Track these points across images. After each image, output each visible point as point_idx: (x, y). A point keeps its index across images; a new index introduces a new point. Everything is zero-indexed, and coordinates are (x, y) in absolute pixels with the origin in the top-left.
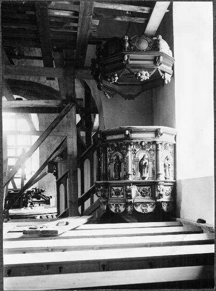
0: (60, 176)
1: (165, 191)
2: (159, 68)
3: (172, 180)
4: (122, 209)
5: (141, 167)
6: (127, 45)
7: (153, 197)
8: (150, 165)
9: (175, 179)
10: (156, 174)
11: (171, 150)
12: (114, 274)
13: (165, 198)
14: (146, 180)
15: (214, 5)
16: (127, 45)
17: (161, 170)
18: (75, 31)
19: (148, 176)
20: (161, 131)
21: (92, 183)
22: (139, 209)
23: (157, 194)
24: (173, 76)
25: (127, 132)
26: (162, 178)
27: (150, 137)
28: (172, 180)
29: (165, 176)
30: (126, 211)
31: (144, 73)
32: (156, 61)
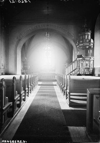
4: (83, 73)
5: (87, 65)
9: (93, 67)
10: (90, 66)
11: (93, 61)
19: (88, 67)
20: (91, 58)
23: (90, 70)
27: (89, 59)
29: (92, 67)
30: (83, 74)
31: (87, 46)
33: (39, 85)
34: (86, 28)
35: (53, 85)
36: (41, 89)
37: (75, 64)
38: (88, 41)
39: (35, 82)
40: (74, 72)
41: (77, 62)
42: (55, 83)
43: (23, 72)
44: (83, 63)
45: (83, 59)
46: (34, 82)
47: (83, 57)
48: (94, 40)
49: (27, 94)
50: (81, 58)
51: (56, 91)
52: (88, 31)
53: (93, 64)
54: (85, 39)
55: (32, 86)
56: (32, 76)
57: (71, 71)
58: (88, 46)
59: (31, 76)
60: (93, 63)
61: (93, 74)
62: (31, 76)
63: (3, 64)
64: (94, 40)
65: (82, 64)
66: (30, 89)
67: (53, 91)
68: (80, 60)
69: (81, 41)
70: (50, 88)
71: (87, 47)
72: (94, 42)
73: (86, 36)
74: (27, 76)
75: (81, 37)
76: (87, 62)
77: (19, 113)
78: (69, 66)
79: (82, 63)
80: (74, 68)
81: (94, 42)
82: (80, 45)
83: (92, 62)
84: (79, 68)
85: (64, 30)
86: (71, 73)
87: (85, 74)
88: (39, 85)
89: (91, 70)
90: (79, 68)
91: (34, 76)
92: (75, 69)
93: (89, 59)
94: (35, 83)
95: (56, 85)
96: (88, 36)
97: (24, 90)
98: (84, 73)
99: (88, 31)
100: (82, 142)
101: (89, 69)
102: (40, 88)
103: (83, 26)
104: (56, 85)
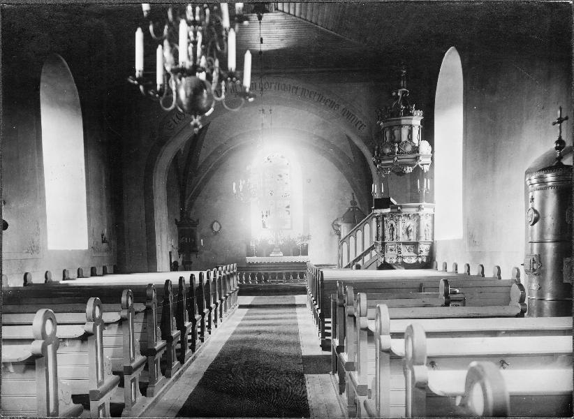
0: (342, 237)
1: (424, 248)
2: (419, 163)
3: (431, 240)
4: (394, 261)
5: (408, 232)
6: (397, 150)
7: (415, 252)
8: (414, 230)
9: (433, 239)
10: (418, 235)
11: (430, 218)
12: (483, 341)
13: (425, 253)
14: (412, 241)
15: (42, 284)
16: (397, 150)
17: (422, 233)
18: (182, 228)
19: (413, 238)
20: (423, 207)
21: (371, 241)
22: (406, 261)
23: (419, 251)
24: (432, 165)
25: (399, 208)
26: (423, 239)
27: (413, 211)
28: (431, 240)
29: (425, 238)
30: (397, 262)
31: (408, 168)
32: (417, 159)
33: (241, 307)
34: (405, 101)
35: (294, 306)
36: (248, 319)
37: (363, 234)
38: (409, 148)
39: (227, 295)
40: (367, 258)
41: (377, 222)
42: (299, 299)
43: (173, 261)
44: (394, 224)
45: (396, 210)
46: (225, 293)
47: (392, 204)
48: (432, 144)
49: (199, 336)
50: (388, 210)
51: (301, 330)
52: (408, 113)
53: (430, 228)
54: (399, 142)
55: (219, 306)
56: (212, 277)
57: (359, 253)
58: (411, 165)
59: (215, 276)
60: (430, 225)
61: (429, 264)
62: (215, 276)
63: (106, 235)
64: (432, 144)
65: (393, 229)
66: (206, 318)
67: (293, 321)
68: (384, 215)
69: (386, 147)
70: (276, 316)
71: (409, 170)
72: (433, 152)
73: (405, 132)
74: (197, 274)
75: (388, 134)
76: (410, 223)
77: (287, 303)
78: (357, 230)
79: (392, 225)
80: (354, 255)
81: (433, 152)
82: (383, 162)
83: (425, 222)
84: (383, 244)
85: (328, 104)
86: (360, 263)
87: (403, 262)
88: (241, 307)
89: (424, 248)
90: (383, 244)
91: (223, 273)
92: (364, 254)
93: (413, 211)
94: (227, 297)
95: (304, 306)
96: (410, 132)
97: (178, 330)
98: (400, 260)
99: (412, 115)
100: (384, 2)
101: (416, 244)
102: (247, 314)
103: (394, 94)
104: (304, 306)
